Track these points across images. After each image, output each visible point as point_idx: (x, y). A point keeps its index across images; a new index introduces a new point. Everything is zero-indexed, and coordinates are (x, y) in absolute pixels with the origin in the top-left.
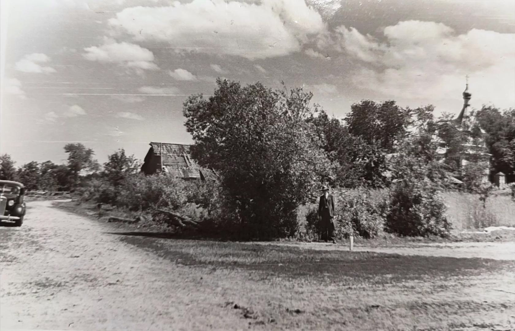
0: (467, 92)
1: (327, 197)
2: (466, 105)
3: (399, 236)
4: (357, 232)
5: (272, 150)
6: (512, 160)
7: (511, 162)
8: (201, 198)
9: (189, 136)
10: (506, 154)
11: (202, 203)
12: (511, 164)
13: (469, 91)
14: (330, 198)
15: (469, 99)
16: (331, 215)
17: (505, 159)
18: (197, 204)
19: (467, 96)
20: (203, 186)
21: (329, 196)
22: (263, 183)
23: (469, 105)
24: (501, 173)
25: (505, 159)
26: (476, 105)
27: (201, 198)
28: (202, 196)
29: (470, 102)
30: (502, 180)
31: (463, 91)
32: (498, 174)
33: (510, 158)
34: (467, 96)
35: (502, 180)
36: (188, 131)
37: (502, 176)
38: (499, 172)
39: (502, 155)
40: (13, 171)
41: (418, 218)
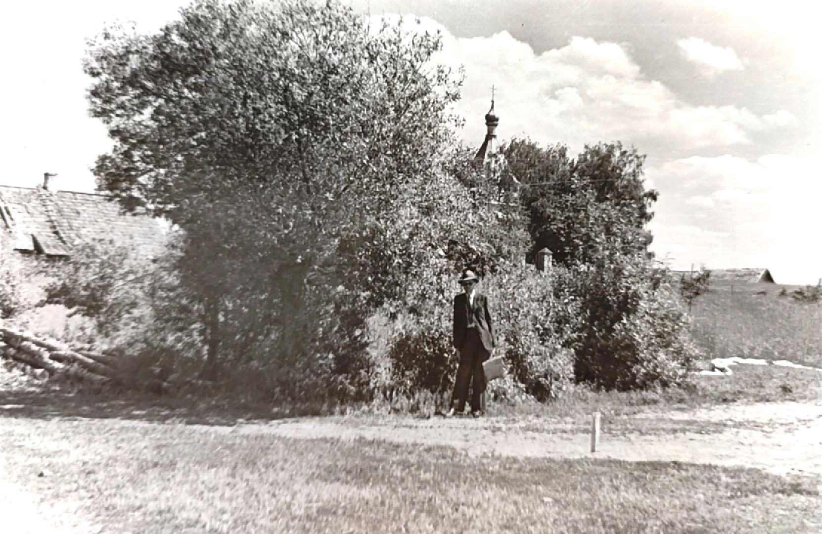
0: (491, 114)
1: (471, 302)
2: (490, 136)
3: (598, 389)
4: (522, 386)
5: (284, 177)
6: (564, 229)
7: (562, 232)
8: (83, 293)
9: (100, 128)
10: (554, 219)
11: (82, 304)
12: (562, 235)
13: (495, 113)
14: (481, 304)
15: (496, 125)
16: (487, 347)
17: (552, 227)
18: (70, 308)
19: (491, 121)
20: (88, 267)
21: (476, 299)
22: (299, 261)
23: (495, 136)
24: (547, 250)
25: (552, 227)
26: (504, 136)
27: (83, 293)
28: (85, 289)
29: (496, 131)
30: (548, 261)
31: (486, 113)
32: (542, 251)
33: (561, 226)
34: (491, 121)
35: (548, 261)
36: (97, 114)
37: (548, 255)
38: (543, 248)
39: (548, 220)
40: (371, 484)
41: (632, 347)
